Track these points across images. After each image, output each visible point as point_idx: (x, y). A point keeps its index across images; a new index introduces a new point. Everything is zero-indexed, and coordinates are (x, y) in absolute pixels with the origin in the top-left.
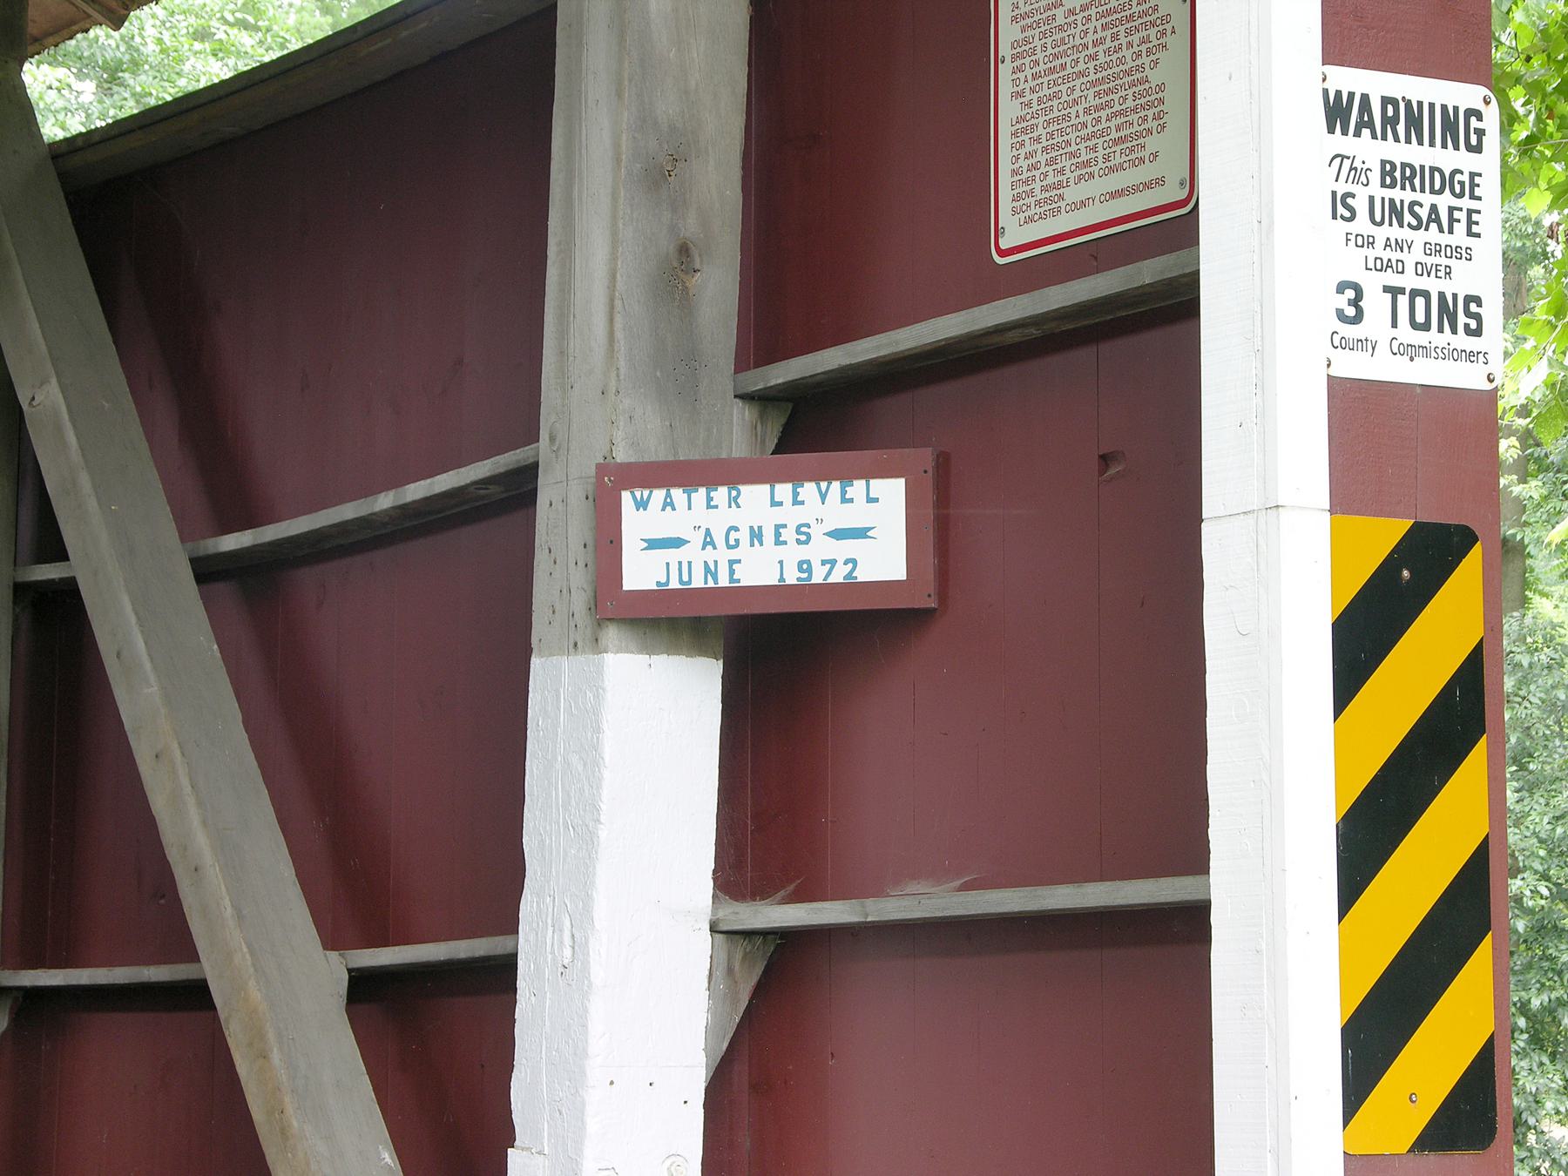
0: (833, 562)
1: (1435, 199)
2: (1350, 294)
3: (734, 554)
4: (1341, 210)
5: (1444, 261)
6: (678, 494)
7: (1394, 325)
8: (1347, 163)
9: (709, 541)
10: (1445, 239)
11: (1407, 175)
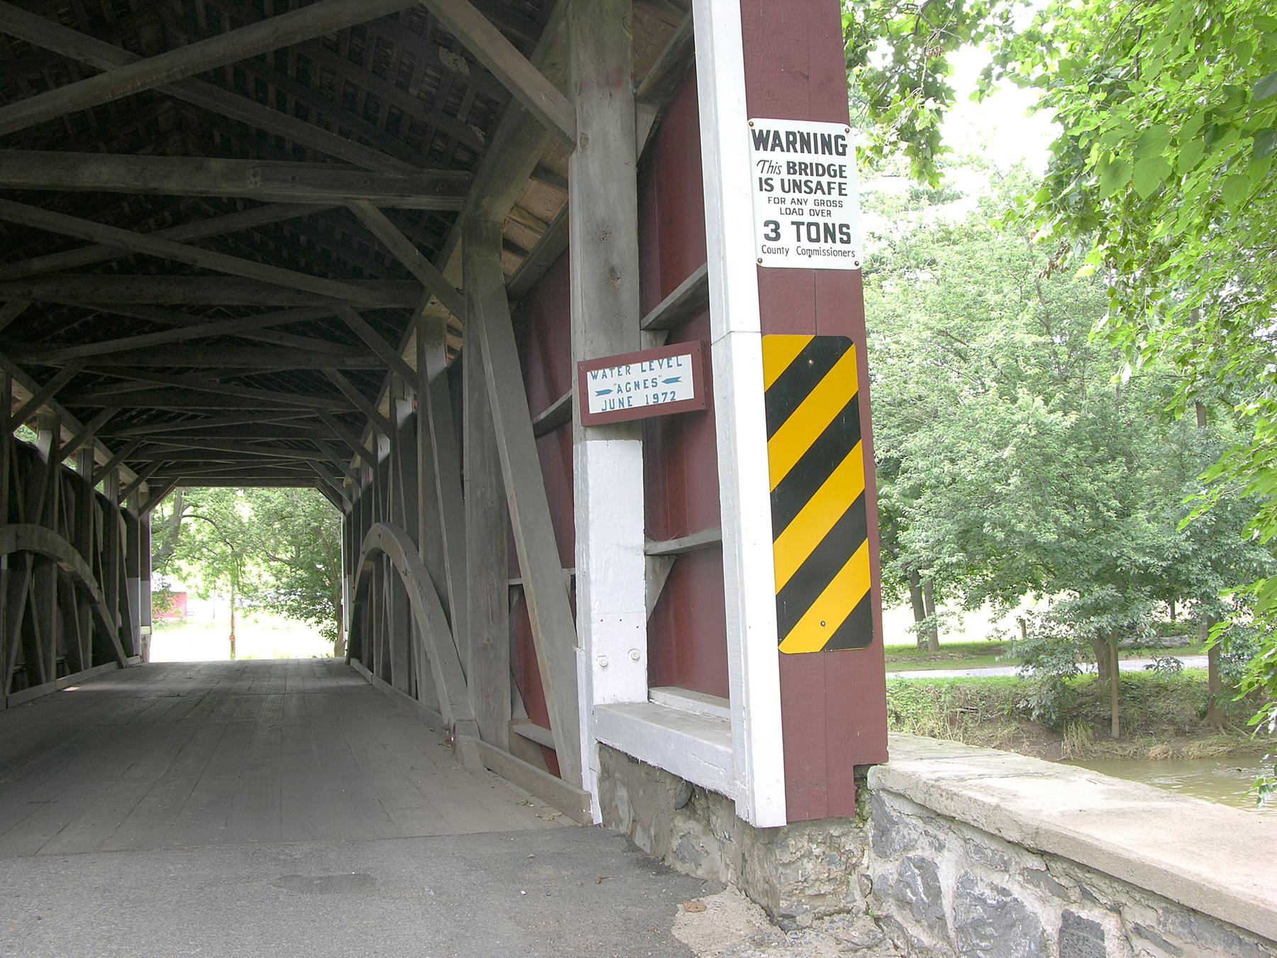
0: (666, 393)
1: (819, 179)
2: (772, 226)
3: (629, 394)
4: (765, 186)
5: (826, 208)
6: (607, 371)
7: (799, 240)
8: (767, 164)
9: (620, 390)
10: (826, 197)
11: (804, 168)
